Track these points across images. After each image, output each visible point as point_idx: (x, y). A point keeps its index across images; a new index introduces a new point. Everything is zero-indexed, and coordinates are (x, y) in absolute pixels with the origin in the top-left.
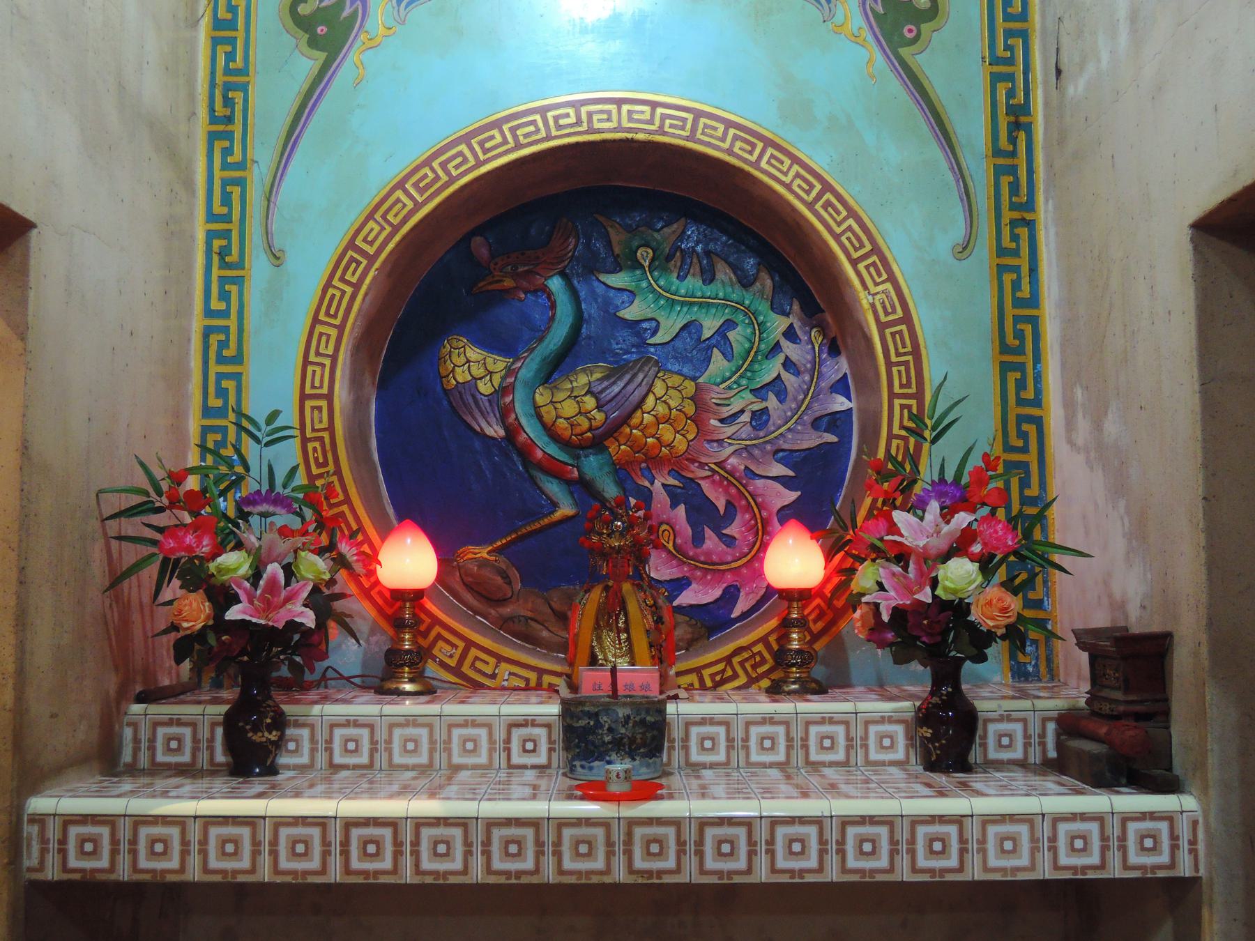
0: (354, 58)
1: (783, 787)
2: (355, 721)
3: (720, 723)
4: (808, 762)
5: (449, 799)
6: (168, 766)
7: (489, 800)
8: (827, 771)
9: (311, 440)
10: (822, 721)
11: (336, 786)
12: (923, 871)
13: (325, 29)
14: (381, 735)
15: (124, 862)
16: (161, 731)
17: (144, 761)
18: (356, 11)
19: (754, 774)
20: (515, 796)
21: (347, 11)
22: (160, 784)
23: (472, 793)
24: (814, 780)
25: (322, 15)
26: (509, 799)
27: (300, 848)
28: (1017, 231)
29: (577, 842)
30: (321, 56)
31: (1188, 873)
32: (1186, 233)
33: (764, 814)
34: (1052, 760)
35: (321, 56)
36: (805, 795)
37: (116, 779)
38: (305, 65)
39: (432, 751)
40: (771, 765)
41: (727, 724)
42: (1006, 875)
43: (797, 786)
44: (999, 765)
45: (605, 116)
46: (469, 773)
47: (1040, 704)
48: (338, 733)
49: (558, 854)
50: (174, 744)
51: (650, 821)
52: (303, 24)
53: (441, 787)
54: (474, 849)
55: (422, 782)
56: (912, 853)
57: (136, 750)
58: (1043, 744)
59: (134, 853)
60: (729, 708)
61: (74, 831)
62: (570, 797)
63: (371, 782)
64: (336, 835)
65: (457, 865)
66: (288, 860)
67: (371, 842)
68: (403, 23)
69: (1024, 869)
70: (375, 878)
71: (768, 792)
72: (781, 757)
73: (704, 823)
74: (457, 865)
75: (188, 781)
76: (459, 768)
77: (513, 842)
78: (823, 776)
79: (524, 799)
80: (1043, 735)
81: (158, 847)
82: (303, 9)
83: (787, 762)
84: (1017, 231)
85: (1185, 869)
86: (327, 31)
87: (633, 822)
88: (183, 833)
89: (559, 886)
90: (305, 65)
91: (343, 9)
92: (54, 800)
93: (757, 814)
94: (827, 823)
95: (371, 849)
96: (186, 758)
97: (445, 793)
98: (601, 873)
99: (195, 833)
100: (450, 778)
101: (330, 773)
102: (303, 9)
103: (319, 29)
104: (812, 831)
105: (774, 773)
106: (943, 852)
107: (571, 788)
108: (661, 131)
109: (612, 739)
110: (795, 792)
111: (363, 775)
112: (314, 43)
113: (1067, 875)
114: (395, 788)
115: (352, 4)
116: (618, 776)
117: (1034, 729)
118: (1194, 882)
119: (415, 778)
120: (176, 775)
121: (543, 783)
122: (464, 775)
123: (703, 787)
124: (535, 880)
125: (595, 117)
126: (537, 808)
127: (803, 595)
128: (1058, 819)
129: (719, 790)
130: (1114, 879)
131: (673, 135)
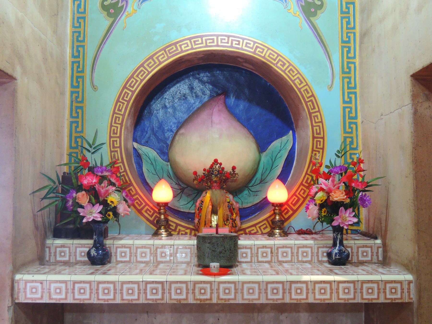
0: (123, 19)
1: (270, 271)
2: (245, 247)
3: (127, 247)
4: (318, 261)
5: (156, 275)
6: (61, 262)
7: (170, 275)
8: (285, 265)
9: (321, 148)
10: (363, 247)
11: (118, 270)
12: (246, 299)
13: (113, 11)
14: (133, 251)
15: (118, 297)
16: (360, 249)
17: (52, 260)
18: (123, 5)
19: (260, 266)
20: (179, 273)
21: (120, 5)
22: (58, 268)
23: (164, 273)
24: (280, 267)
25: (114, 5)
26: (177, 275)
27: (275, 291)
28: (77, 84)
29: (152, 289)
30: (112, 20)
31: (407, 301)
32: (405, 85)
33: (168, 280)
34: (380, 261)
35: (112, 20)
36: (278, 274)
37: (43, 267)
38: (106, 22)
39: (251, 257)
40: (266, 262)
41: (291, 248)
42: (274, 301)
43: (275, 270)
44: (57, 263)
45: (211, 41)
46: (163, 264)
47: (357, 242)
48: (280, 250)
49: (290, 293)
50: (365, 254)
51: (225, 282)
52: (104, 8)
53: (154, 271)
54: (69, 291)
55: (147, 268)
56: (242, 293)
57: (50, 256)
58: (377, 256)
59: (122, 293)
60: (292, 242)
61: (77, 286)
62: (198, 274)
63: (130, 268)
64: (191, 287)
65: (375, 296)
66: (150, 295)
67: (227, 289)
68: (140, 9)
69: (232, 299)
70: (107, 301)
71: (265, 273)
72: (309, 259)
73: (244, 283)
74: (136, 297)
75: (67, 268)
76: (159, 263)
77: (275, 289)
78: (284, 267)
79: (182, 275)
80: (377, 253)
81: (299, 291)
82: (106, 3)
83: (312, 260)
84: (77, 84)
85: (406, 300)
86: (114, 11)
87: (220, 283)
88: (90, 286)
89: (291, 304)
90: (106, 22)
91: (118, 5)
92: (22, 275)
93: (141, 280)
94: (189, 283)
95: (227, 291)
96: (67, 259)
97: (155, 273)
98: (184, 299)
99: (334, 286)
100: (156, 267)
101: (130, 264)
102: (106, 3)
103: (111, 11)
104: (184, 286)
105: (267, 265)
106: (253, 293)
107: (198, 271)
108: (232, 47)
109: (219, 254)
110: (274, 273)
111: (126, 266)
112: (109, 15)
113: (247, 302)
114: (138, 271)
115: (122, 2)
116: (214, 267)
117: (375, 251)
118: (409, 305)
119: (145, 267)
120: (63, 265)
121: (188, 269)
122: (161, 266)
123: (243, 271)
124: (185, 302)
125: (208, 41)
126: (187, 278)
127: (281, 205)
128: (363, 282)
129: (248, 272)
130: (358, 303)
131: (188, 50)
